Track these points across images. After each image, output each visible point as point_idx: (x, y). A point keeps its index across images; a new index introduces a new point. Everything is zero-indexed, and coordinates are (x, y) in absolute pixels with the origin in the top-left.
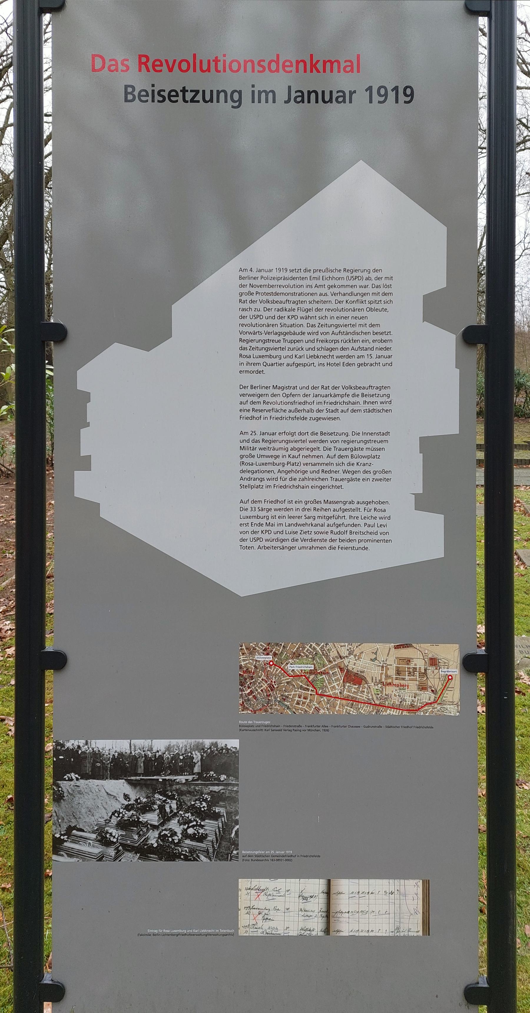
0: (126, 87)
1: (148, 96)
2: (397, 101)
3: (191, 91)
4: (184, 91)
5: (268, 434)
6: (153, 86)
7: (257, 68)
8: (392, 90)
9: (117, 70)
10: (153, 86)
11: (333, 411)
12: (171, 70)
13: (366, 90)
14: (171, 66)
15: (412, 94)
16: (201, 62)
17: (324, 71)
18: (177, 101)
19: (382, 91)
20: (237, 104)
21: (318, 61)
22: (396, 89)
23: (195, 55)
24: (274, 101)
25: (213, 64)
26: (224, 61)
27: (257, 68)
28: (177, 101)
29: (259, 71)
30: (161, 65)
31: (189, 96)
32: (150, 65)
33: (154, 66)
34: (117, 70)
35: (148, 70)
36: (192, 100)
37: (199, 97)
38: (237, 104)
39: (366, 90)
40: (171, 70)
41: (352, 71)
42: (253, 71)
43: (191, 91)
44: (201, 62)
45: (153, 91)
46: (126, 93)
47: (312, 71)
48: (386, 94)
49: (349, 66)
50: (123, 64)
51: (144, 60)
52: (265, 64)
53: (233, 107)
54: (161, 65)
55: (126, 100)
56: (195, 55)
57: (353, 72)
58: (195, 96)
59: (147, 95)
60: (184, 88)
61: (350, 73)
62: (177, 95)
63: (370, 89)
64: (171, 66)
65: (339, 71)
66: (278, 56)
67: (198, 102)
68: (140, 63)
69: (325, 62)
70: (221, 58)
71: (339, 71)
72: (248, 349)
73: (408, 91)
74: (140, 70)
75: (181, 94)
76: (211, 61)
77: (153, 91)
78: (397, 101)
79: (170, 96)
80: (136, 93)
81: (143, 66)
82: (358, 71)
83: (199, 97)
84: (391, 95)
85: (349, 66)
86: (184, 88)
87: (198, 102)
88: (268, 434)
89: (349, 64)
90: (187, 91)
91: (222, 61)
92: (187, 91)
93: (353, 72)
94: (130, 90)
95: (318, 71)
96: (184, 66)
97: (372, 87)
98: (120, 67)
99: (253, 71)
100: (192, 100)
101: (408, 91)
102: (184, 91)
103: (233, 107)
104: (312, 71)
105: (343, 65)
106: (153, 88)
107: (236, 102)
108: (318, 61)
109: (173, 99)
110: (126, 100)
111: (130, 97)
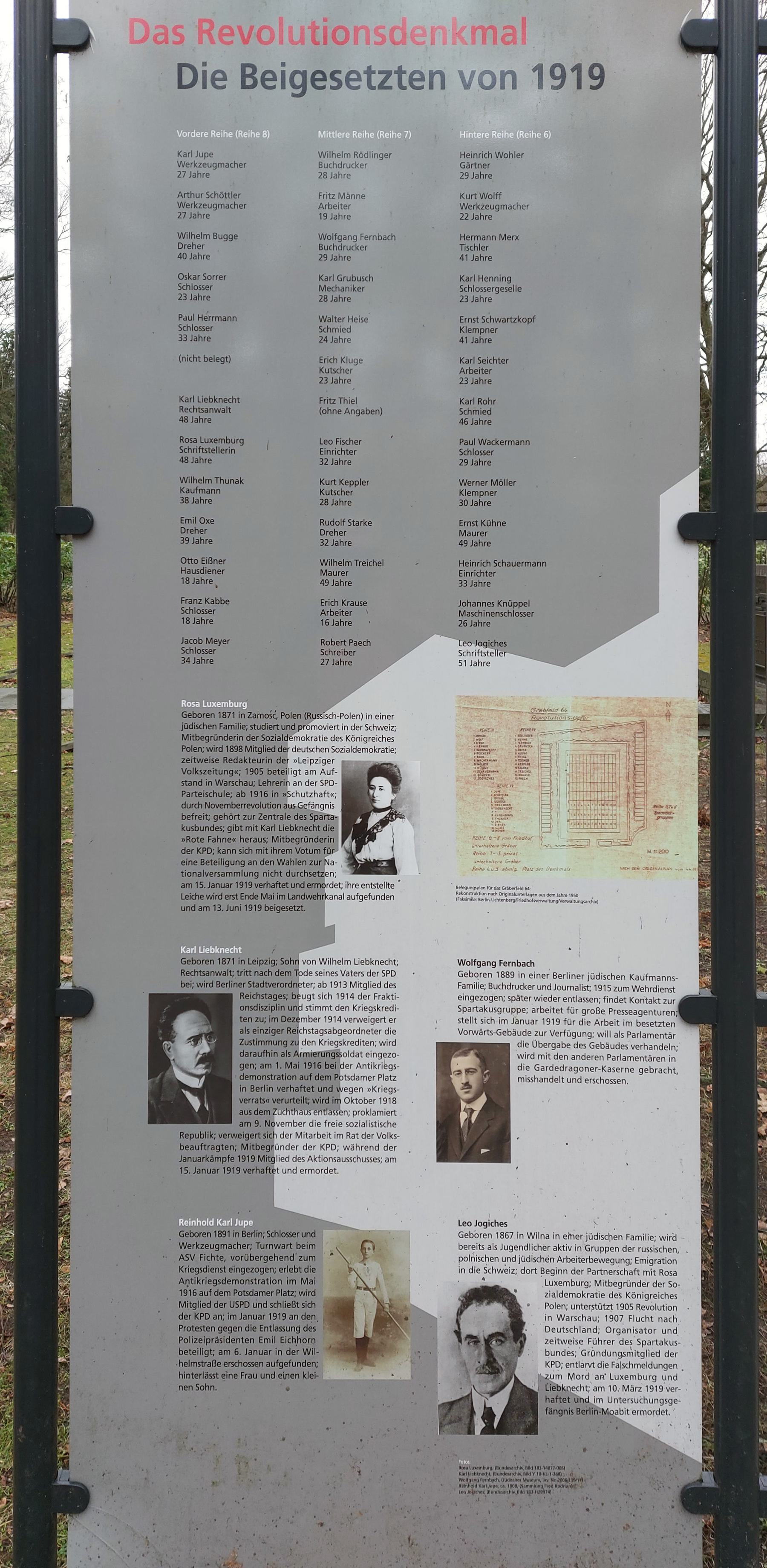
0: (244, 66)
1: (276, 80)
2: (579, 87)
3: (380, 72)
4: (369, 72)
5: (206, 1171)
6: (283, 64)
7: (374, 38)
8: (573, 70)
9: (166, 41)
10: (283, 64)
11: (258, 985)
12: (246, 41)
13: (534, 70)
14: (246, 36)
15: (602, 76)
16: (291, 29)
17: (474, 42)
18: (358, 87)
19: (558, 72)
20: (299, 91)
21: (463, 28)
22: (578, 68)
23: (281, 19)
24: (514, 87)
25: (308, 33)
26: (325, 28)
27: (374, 38)
28: (358, 87)
29: (376, 43)
30: (232, 34)
31: (376, 79)
32: (215, 33)
33: (221, 35)
34: (166, 41)
35: (212, 42)
36: (382, 86)
37: (393, 81)
38: (299, 91)
39: (534, 70)
40: (246, 41)
41: (514, 41)
42: (368, 43)
43: (380, 72)
44: (291, 28)
45: (283, 73)
46: (244, 76)
47: (454, 43)
48: (563, 76)
49: (162, 34)
50: (377, 33)
51: (206, 26)
52: (386, 32)
53: (294, 95)
54: (232, 34)
55: (244, 86)
56: (281, 19)
57: (515, 43)
58: (384, 82)
59: (274, 79)
60: (369, 67)
61: (163, 45)
62: (359, 79)
63: (539, 68)
64: (246, 36)
65: (495, 42)
66: (404, 20)
67: (390, 88)
68: (201, 32)
69: (474, 30)
70: (320, 23)
71: (495, 42)
72: (247, 716)
73: (597, 72)
74: (200, 41)
75: (364, 77)
76: (306, 28)
77: (283, 73)
78: (579, 87)
79: (348, 80)
80: (258, 76)
81: (205, 37)
82: (524, 43)
83: (393, 81)
84: (571, 77)
85: (162, 34)
86: (369, 67)
87: (390, 88)
88: (206, 1171)
89: (510, 31)
90: (374, 72)
91: (321, 28)
92: (374, 72)
93: (515, 43)
94: (249, 71)
95: (464, 42)
96: (266, 35)
97: (542, 65)
98: (172, 37)
99: (368, 43)
100: (382, 86)
101: (597, 72)
102: (369, 72)
103: (294, 95)
104: (454, 43)
105: (500, 33)
106: (283, 68)
107: (298, 87)
108: (463, 28)
109: (268, 83)
110: (244, 86)
111: (249, 81)
